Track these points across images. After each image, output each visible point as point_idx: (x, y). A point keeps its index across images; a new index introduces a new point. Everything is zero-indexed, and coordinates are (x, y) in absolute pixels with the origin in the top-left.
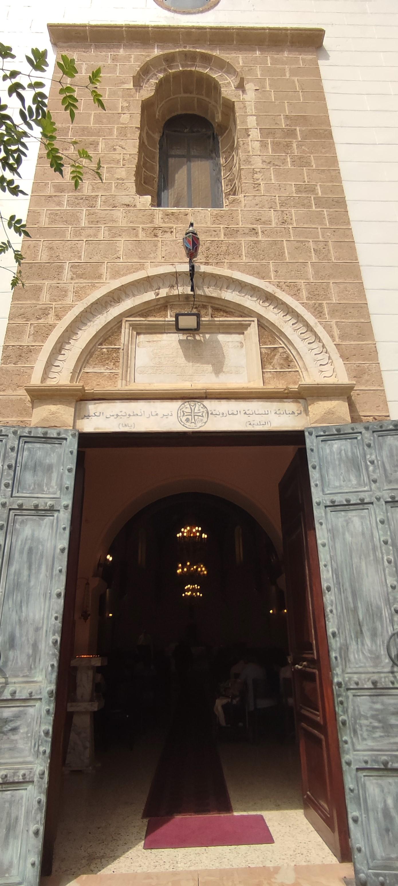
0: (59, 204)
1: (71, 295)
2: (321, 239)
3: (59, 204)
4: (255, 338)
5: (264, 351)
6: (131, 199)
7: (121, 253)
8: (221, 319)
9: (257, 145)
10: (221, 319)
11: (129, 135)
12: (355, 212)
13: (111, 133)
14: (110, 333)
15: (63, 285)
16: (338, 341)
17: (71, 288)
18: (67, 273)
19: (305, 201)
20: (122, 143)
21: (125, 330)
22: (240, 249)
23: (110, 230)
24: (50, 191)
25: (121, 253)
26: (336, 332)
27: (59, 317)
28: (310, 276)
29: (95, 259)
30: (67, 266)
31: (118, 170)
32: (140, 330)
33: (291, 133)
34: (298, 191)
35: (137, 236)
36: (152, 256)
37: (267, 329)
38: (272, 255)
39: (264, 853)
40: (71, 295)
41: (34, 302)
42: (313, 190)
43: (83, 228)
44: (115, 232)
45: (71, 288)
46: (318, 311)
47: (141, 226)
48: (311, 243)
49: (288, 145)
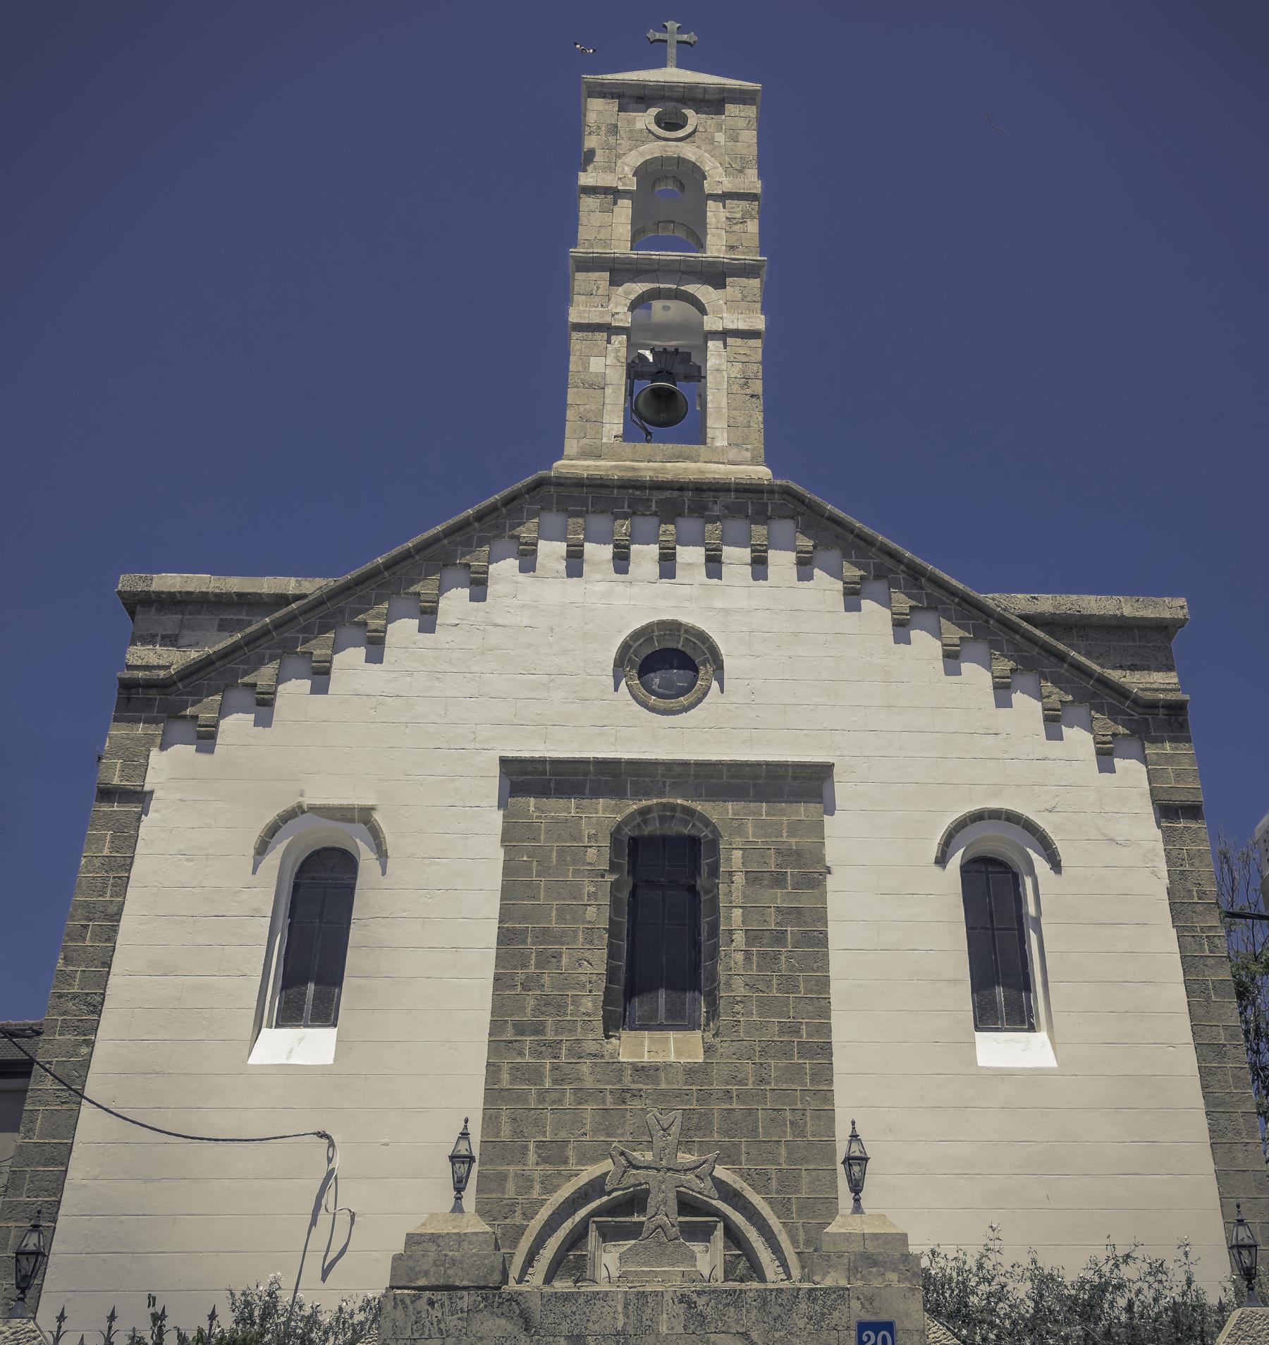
0: (521, 1054)
1: (537, 1187)
2: (799, 1106)
3: (521, 1054)
4: (720, 1245)
5: (728, 1258)
6: (598, 1046)
7: (588, 1127)
8: (1083, 659)
9: (739, 957)
10: (1083, 659)
11: (596, 942)
12: (841, 1063)
13: (575, 939)
14: (577, 1238)
15: (528, 1173)
16: (802, 1248)
17: (536, 1176)
18: (532, 1157)
19: (788, 1048)
20: (587, 954)
21: (593, 1235)
22: (711, 1123)
23: (575, 1094)
24: (509, 1035)
25: (588, 1127)
26: (801, 1236)
27: (528, 1216)
28: (782, 1160)
29: (562, 1135)
30: (531, 1146)
31: (584, 1000)
32: (608, 1235)
33: (779, 937)
34: (781, 1033)
35: (604, 1102)
36: (619, 1131)
37: (734, 1237)
38: (745, 1130)
39: (738, 1008)
40: (537, 1187)
41: (500, 1195)
42: (797, 1032)
43: (547, 1090)
44: (582, 1095)
45: (536, 1176)
46: (782, 1208)
47: (608, 1087)
48: (788, 1113)
49: (776, 958)
